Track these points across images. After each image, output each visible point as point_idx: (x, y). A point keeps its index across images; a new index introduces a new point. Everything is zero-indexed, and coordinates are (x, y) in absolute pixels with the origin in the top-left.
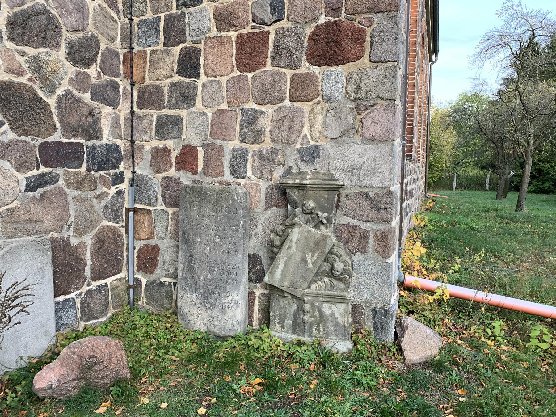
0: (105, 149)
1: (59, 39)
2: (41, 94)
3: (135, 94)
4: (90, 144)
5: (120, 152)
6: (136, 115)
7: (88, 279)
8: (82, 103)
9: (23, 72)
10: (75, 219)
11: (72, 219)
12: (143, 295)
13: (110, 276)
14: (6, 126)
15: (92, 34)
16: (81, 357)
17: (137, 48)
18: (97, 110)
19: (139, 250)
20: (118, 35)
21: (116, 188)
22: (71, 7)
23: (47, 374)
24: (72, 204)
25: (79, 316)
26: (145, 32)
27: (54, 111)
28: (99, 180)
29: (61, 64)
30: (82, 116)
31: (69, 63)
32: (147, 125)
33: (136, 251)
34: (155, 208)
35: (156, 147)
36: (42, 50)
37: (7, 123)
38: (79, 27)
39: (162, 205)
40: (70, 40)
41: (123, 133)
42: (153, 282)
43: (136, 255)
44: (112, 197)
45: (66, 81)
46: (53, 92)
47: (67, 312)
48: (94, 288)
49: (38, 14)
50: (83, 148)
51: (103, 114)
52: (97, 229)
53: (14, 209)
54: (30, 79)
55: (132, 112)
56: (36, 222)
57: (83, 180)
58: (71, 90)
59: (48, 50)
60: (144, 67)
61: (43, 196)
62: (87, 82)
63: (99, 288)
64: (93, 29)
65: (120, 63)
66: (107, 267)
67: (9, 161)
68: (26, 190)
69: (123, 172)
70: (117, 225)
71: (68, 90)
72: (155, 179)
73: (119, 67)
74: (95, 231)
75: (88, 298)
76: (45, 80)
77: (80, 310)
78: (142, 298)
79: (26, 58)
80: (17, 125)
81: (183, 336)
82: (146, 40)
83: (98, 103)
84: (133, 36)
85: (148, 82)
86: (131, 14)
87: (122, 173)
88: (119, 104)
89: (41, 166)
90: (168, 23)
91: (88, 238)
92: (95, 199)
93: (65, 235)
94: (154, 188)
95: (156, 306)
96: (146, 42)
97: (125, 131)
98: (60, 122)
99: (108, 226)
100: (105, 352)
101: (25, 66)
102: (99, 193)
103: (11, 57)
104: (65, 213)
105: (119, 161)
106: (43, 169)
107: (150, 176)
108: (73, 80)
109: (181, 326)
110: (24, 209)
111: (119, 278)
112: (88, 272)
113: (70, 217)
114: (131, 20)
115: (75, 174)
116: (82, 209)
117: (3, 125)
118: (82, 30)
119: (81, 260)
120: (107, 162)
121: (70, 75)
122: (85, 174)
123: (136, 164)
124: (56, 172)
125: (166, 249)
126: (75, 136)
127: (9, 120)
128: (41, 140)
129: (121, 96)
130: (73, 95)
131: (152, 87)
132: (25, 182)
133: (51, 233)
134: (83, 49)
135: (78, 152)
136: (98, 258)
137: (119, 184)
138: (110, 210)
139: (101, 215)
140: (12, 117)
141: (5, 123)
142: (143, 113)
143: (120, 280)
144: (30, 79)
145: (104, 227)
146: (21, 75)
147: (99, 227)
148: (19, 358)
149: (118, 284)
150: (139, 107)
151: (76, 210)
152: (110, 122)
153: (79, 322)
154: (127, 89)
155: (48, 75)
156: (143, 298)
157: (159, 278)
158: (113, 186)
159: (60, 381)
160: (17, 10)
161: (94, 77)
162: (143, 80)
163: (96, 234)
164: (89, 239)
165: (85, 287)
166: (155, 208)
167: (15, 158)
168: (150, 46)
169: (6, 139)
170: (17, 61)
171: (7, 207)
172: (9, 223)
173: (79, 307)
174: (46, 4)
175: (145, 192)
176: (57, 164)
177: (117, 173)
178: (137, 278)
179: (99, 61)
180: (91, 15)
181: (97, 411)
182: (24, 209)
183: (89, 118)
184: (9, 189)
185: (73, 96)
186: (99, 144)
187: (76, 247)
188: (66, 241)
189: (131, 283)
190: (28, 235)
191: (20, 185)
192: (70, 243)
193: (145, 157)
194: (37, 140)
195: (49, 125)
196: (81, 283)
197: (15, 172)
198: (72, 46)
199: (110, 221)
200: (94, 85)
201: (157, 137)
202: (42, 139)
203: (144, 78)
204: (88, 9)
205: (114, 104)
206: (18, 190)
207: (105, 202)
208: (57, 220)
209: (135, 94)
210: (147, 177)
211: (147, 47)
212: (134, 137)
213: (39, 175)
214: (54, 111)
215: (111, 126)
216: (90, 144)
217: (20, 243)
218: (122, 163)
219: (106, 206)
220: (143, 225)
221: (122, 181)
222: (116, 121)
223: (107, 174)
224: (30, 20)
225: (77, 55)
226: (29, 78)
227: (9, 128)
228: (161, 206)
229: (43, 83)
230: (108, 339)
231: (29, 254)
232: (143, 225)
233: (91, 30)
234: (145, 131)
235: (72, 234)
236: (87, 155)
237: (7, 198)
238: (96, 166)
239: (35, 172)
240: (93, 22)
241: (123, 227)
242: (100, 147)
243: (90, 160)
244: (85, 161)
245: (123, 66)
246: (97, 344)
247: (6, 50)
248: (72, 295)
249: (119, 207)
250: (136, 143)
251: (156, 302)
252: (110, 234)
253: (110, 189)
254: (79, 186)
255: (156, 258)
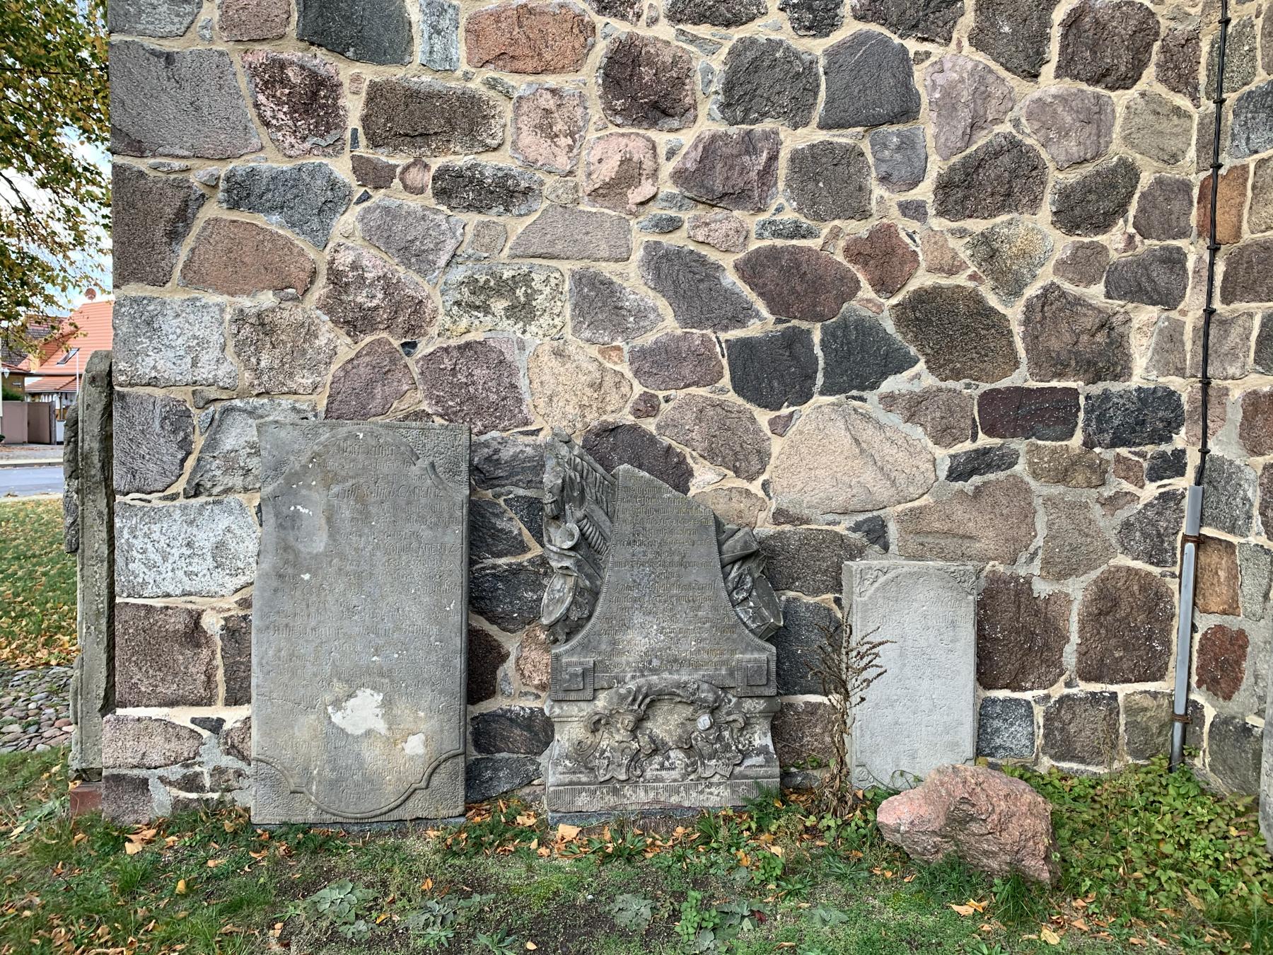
0: (1135, 400)
1: (1037, 190)
2: (993, 301)
3: (1220, 268)
4: (1097, 389)
5: (1179, 406)
6: (1217, 317)
7: (1068, 673)
8: (1081, 305)
9: (961, 265)
10: (1046, 542)
11: (1039, 541)
12: (1205, 744)
13: (1128, 681)
14: (921, 366)
15: (1120, 159)
16: (950, 795)
17: (1227, 161)
18: (1121, 318)
19: (1205, 635)
20: (1189, 145)
21: (1160, 487)
22: (1068, 119)
23: (901, 804)
24: (1041, 511)
25: (1039, 741)
26: (1246, 123)
27: (1017, 330)
28: (1113, 466)
29: (1040, 237)
30: (1082, 332)
31: (1058, 232)
32: (1238, 340)
33: (1197, 637)
34: (1243, 540)
35: (1255, 392)
36: (1004, 217)
37: (923, 360)
38: (1086, 154)
39: (1258, 534)
40: (1063, 186)
41: (1188, 363)
42: (1227, 721)
43: (1196, 646)
44: (1146, 505)
45: (1049, 267)
46: (1017, 293)
47: (1012, 724)
48: (1082, 695)
49: (997, 154)
50: (1078, 398)
51: (1135, 324)
52: (1100, 570)
53: (921, 510)
54: (973, 277)
55: (1209, 312)
56: (964, 537)
57: (1073, 464)
58: (1058, 283)
59: (1015, 215)
60: (1241, 204)
61: (980, 491)
62: (1099, 262)
63: (1094, 698)
64: (1123, 148)
65: (1191, 203)
66: (1121, 658)
67: (921, 425)
68: (948, 478)
69: (1183, 452)
70: (1156, 571)
71: (1053, 283)
72: (1247, 470)
73: (1188, 214)
74: (1094, 574)
75: (1063, 712)
76: (1002, 272)
77: (1042, 731)
78: (1201, 753)
79: (968, 239)
80: (942, 362)
81: (1255, 870)
82: (1248, 139)
83: (1122, 303)
84: (1222, 137)
85: (1247, 236)
86: (1220, 89)
87: (1180, 454)
88: (1182, 297)
89: (981, 434)
90: (676, 283)
91: (1076, 586)
92: (1098, 506)
93: (1022, 572)
94: (1244, 490)
95: (1230, 781)
96: (1247, 144)
97: (1192, 358)
98: (1027, 351)
99: (1129, 569)
100: (999, 806)
101: (964, 255)
102: (1112, 493)
103: (940, 244)
104: (1024, 527)
105: (1174, 425)
106: (984, 441)
107: (1237, 462)
108: (1065, 262)
109: (1262, 843)
110: (940, 511)
111: (1153, 690)
112: (1070, 656)
113: (1035, 536)
114: (1220, 102)
115: (1054, 451)
116: (1065, 523)
117: (916, 363)
118: (1093, 158)
119: (1056, 629)
120: (1138, 428)
121: (1058, 255)
122: (1078, 451)
123: (1210, 432)
124: (1013, 446)
125: (1262, 645)
126: (1060, 375)
127: (927, 354)
128: (985, 387)
129: (1191, 279)
130: (1064, 293)
131: (1255, 248)
132: (948, 462)
133: (991, 563)
134: (1092, 197)
135: (1065, 407)
136: (1099, 633)
137: (1169, 478)
138: (1138, 534)
139: (1113, 541)
140: (932, 349)
141: (919, 360)
142: (1233, 311)
143: (1155, 695)
144: (973, 277)
145: (1118, 569)
146: (957, 272)
147: (1104, 567)
148: (899, 773)
149: (1148, 702)
150: (1226, 300)
151: (1050, 525)
152: (1154, 340)
153: (1037, 755)
154: (1205, 261)
155: (1009, 262)
156: (1204, 752)
157: (1243, 714)
158: (1152, 480)
159: (914, 825)
160: (955, 159)
161: (1116, 249)
162: (1238, 235)
163: (1095, 581)
164: (1077, 590)
165: (1061, 687)
166: (1243, 540)
167: (933, 419)
168: (1256, 152)
169: (919, 386)
170: (949, 249)
171: (910, 505)
172: (911, 532)
173: (1041, 724)
174: (1014, 132)
175: (1224, 499)
176: (1015, 430)
177: (1164, 452)
178: (1195, 702)
179: (1132, 210)
180: (1119, 122)
181: (956, 908)
182: (940, 511)
183: (1099, 335)
184: (917, 474)
185: (1063, 294)
186: (1118, 389)
187: (1047, 601)
188: (1023, 584)
189: (1180, 710)
190: (945, 559)
191: (938, 467)
192: (1031, 590)
193: (1229, 415)
194: (977, 386)
195: (1004, 356)
196: (1051, 677)
197: (930, 444)
198: (1068, 196)
199: (1137, 559)
200: (1116, 265)
201: (1257, 368)
202: (988, 385)
203: (1239, 228)
204: (1113, 111)
205: (1169, 300)
206: (933, 476)
207: (1122, 515)
208: (1007, 540)
209: (1220, 268)
210: (1231, 465)
211: (1249, 156)
212: (1209, 368)
213: (976, 451)
214: (1017, 330)
215: (1155, 349)
216: (1097, 389)
217: (916, 569)
218: (1183, 430)
219: (1127, 525)
220: (1216, 577)
221: (1181, 472)
222: (1171, 337)
223: (1135, 453)
224: (980, 170)
225: (1077, 211)
226: (970, 276)
227: (925, 367)
228: (1258, 537)
229: (997, 280)
230: (1023, 787)
231: (932, 593)
232: (1216, 577)
233: (1117, 149)
234: (1232, 355)
235: (1037, 572)
236: (1087, 412)
237: (911, 490)
238: (1107, 437)
239: (968, 446)
240: (1123, 134)
241: (1173, 575)
242: (1121, 396)
243: (1094, 422)
244: (1081, 424)
245: (1198, 209)
246: (990, 785)
247: (931, 233)
248: (1028, 696)
249: (1166, 529)
250: (1214, 383)
251: (1232, 770)
252: (1136, 588)
253: (1142, 487)
254: (1062, 476)
255: (1238, 663)
